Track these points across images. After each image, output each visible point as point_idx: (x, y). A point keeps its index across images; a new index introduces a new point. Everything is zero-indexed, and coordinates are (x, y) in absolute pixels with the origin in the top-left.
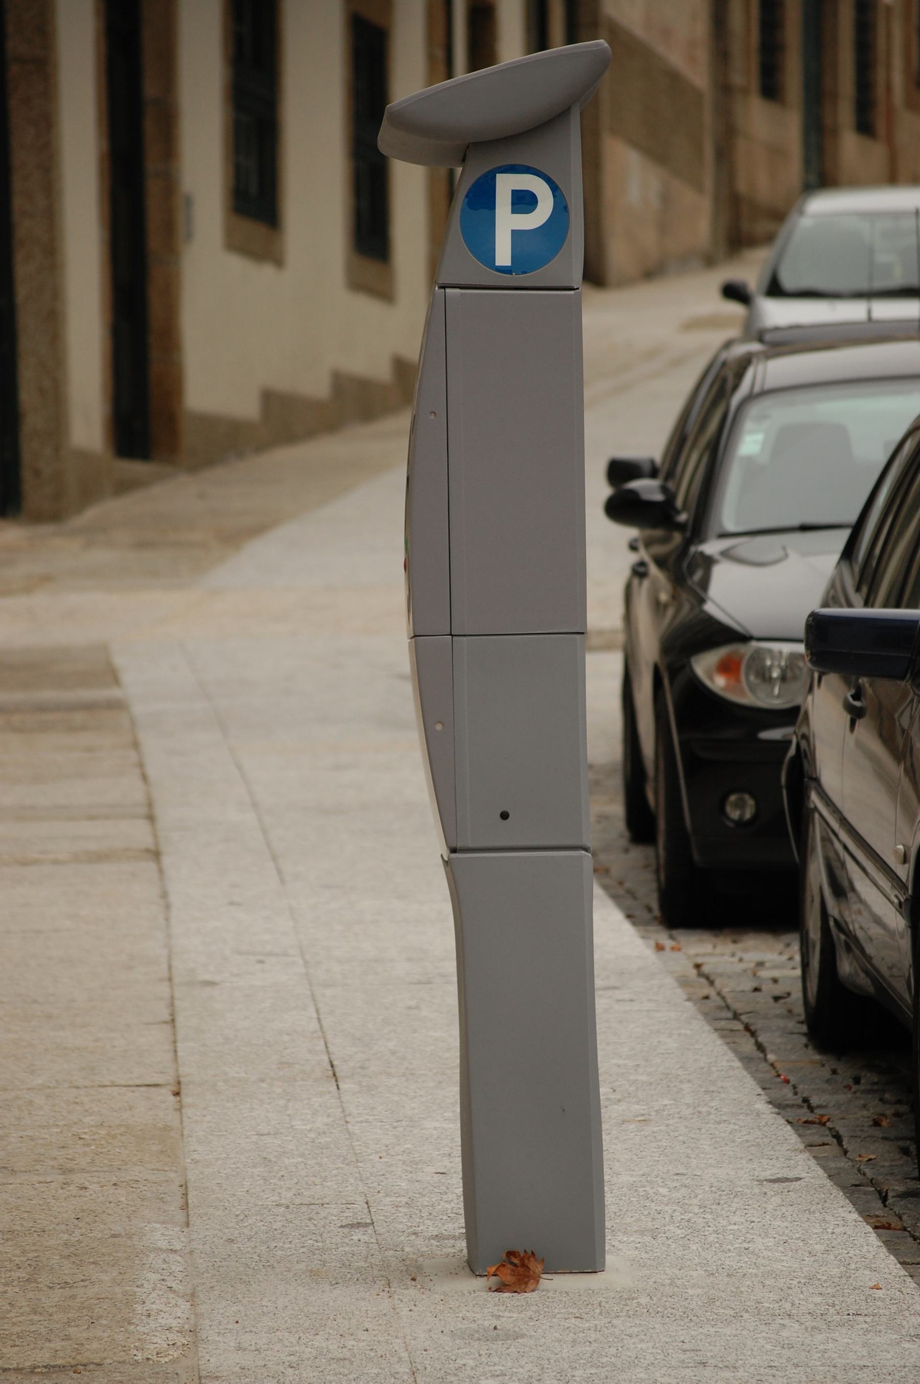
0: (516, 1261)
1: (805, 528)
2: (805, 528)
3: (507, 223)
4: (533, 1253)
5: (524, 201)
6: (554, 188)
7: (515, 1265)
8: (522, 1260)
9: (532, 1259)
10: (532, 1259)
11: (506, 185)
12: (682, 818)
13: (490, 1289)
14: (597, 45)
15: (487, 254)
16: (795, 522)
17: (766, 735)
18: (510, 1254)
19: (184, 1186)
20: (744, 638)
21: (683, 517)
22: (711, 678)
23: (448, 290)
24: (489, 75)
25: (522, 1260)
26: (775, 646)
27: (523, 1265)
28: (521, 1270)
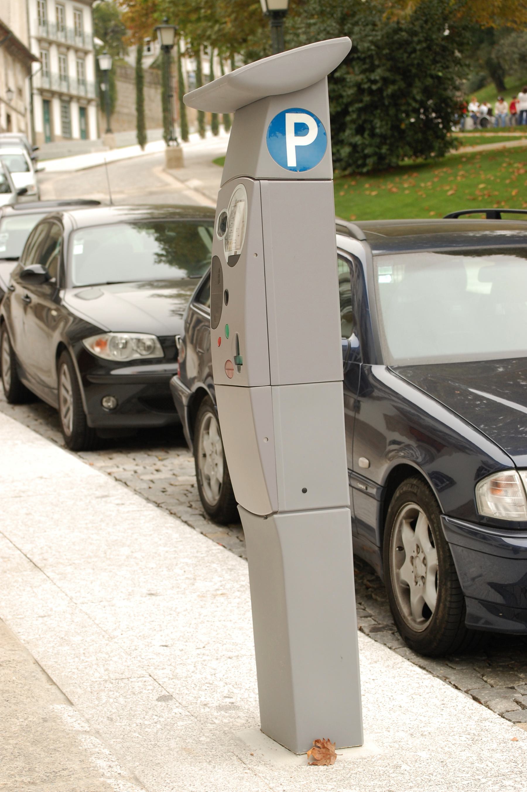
0: (319, 745)
1: (109, 283)
2: (109, 283)
3: (292, 142)
4: (329, 740)
5: (301, 129)
6: (318, 122)
7: (319, 747)
8: (323, 744)
9: (328, 743)
10: (328, 743)
11: (291, 119)
12: (82, 407)
13: (309, 763)
14: (346, 39)
15: (282, 161)
16: (105, 281)
17: (114, 372)
18: (317, 741)
19: (36, 662)
20: (105, 332)
21: (53, 280)
22: (93, 348)
23: (261, 181)
24: (287, 55)
25: (323, 744)
26: (119, 335)
27: (324, 747)
28: (324, 750)
